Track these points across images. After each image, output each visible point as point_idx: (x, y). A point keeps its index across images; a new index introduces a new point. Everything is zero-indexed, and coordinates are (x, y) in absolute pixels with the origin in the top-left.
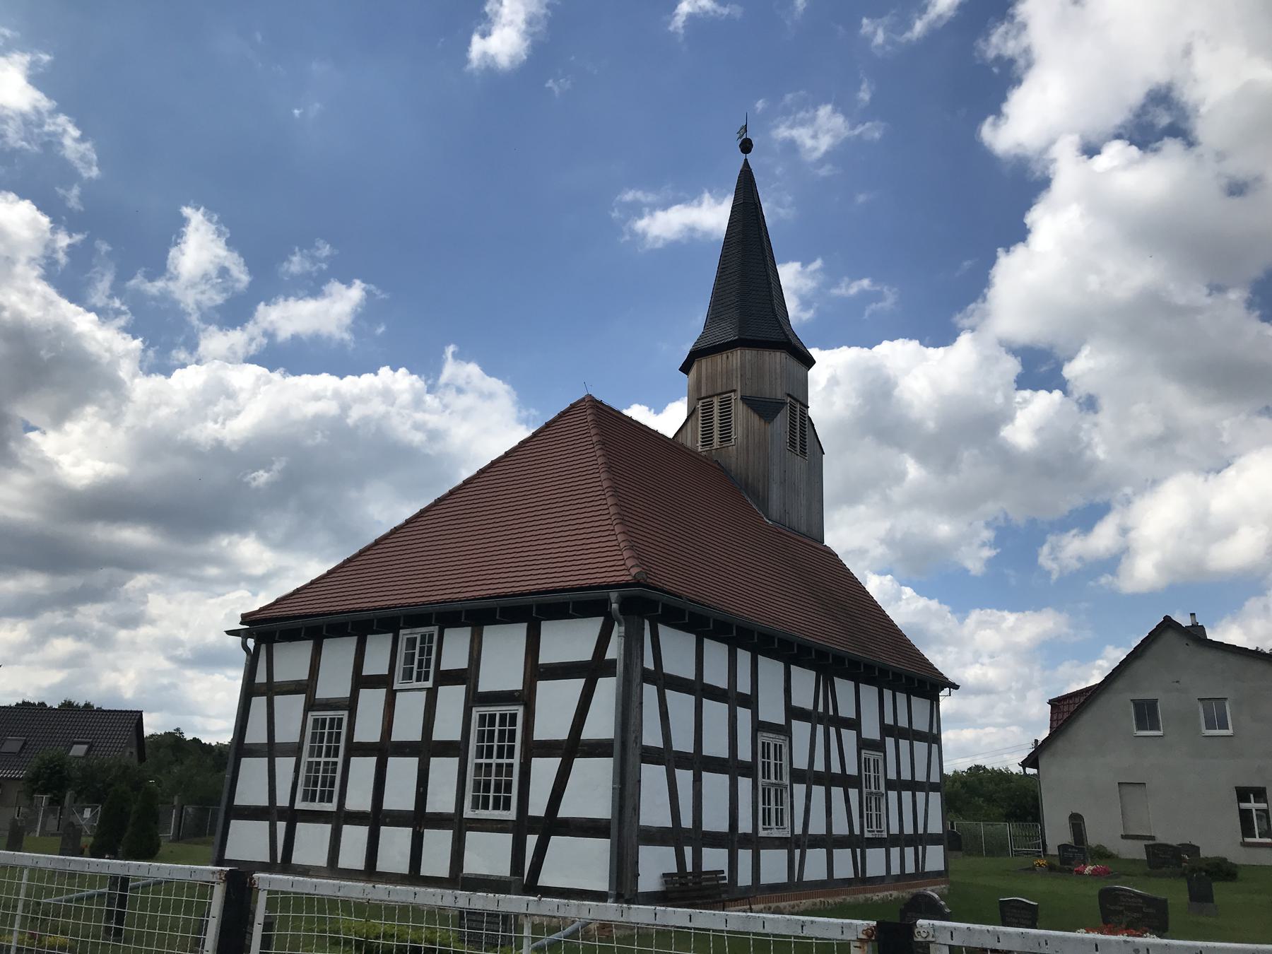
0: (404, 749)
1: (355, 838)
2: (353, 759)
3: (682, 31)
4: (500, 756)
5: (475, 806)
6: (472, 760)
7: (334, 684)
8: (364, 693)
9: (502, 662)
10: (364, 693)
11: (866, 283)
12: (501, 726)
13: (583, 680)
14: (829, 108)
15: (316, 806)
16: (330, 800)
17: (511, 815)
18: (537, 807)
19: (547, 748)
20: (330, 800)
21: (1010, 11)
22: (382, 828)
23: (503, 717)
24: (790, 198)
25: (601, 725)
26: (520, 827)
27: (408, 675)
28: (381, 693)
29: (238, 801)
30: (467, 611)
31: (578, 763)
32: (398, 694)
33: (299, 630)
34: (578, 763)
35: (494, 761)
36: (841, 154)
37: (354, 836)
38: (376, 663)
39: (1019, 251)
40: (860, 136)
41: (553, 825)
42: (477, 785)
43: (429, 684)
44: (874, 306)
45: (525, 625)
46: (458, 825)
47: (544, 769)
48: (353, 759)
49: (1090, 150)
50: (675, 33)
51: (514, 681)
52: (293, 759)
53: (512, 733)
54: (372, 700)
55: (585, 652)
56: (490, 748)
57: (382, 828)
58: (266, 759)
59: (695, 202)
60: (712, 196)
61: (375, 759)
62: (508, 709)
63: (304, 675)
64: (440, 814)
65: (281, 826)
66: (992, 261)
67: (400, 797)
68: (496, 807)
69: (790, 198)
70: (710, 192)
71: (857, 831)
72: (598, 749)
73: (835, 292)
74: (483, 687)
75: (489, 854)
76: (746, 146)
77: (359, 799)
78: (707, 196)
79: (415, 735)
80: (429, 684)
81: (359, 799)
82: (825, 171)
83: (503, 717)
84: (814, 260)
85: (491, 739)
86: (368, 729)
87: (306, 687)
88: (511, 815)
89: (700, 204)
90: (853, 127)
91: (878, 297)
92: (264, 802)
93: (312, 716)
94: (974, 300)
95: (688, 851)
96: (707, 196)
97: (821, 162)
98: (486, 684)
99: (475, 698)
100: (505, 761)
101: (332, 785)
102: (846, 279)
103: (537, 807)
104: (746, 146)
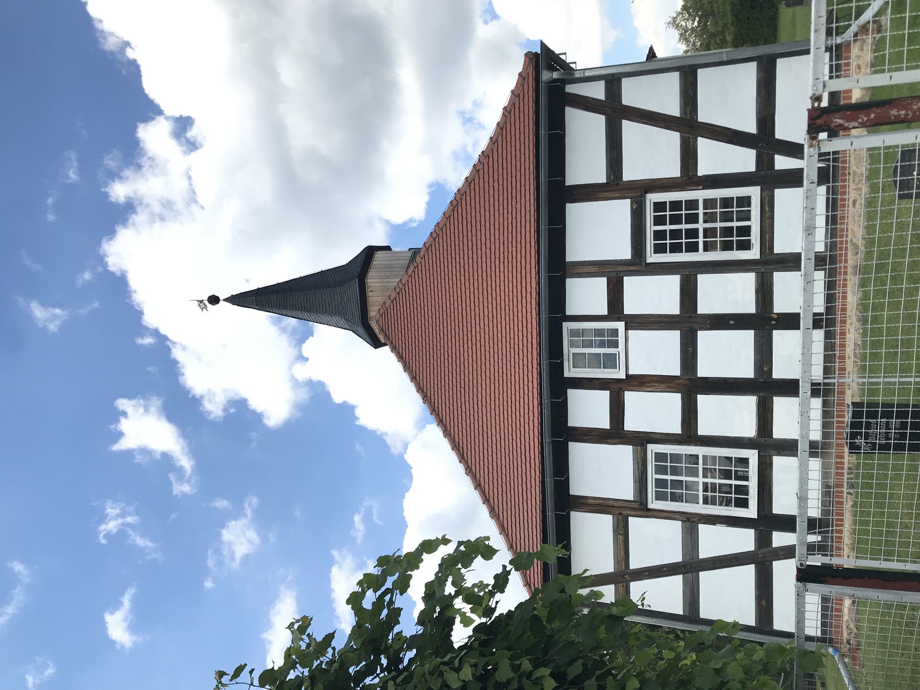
2: (701, 432)
3: (134, 638)
5: (744, 504)
6: (701, 256)
8: (631, 424)
10: (631, 424)
11: (357, 518)
14: (224, 532)
17: (752, 455)
18: (743, 160)
20: (744, 462)
21: (198, 396)
22: (776, 375)
24: (282, 571)
26: (769, 179)
27: (610, 361)
28: (631, 398)
29: (751, 621)
30: (556, 510)
31: (704, 116)
32: (631, 372)
34: (704, 116)
36: (262, 522)
39: (358, 412)
40: (253, 511)
41: (764, 140)
43: (620, 326)
44: (375, 517)
45: (569, 390)
48: (701, 432)
49: (302, 358)
50: (135, 644)
51: (621, 209)
52: (702, 527)
55: (596, 123)
57: (776, 375)
58: (703, 575)
59: (267, 646)
60: (267, 631)
61: (700, 174)
66: (363, 429)
69: (282, 571)
70: (263, 632)
72: (689, 156)
73: (359, 539)
74: (625, 253)
75: (796, 219)
76: (214, 300)
78: (265, 636)
80: (620, 326)
82: (272, 538)
84: (333, 556)
87: (620, 513)
88: (752, 455)
89: (270, 642)
90: (246, 515)
91: (369, 511)
92: (748, 572)
93: (654, 504)
94: (384, 441)
96: (265, 636)
97: (264, 539)
98: (626, 491)
99: (638, 265)
102: (352, 532)
103: (743, 160)
104: (214, 300)
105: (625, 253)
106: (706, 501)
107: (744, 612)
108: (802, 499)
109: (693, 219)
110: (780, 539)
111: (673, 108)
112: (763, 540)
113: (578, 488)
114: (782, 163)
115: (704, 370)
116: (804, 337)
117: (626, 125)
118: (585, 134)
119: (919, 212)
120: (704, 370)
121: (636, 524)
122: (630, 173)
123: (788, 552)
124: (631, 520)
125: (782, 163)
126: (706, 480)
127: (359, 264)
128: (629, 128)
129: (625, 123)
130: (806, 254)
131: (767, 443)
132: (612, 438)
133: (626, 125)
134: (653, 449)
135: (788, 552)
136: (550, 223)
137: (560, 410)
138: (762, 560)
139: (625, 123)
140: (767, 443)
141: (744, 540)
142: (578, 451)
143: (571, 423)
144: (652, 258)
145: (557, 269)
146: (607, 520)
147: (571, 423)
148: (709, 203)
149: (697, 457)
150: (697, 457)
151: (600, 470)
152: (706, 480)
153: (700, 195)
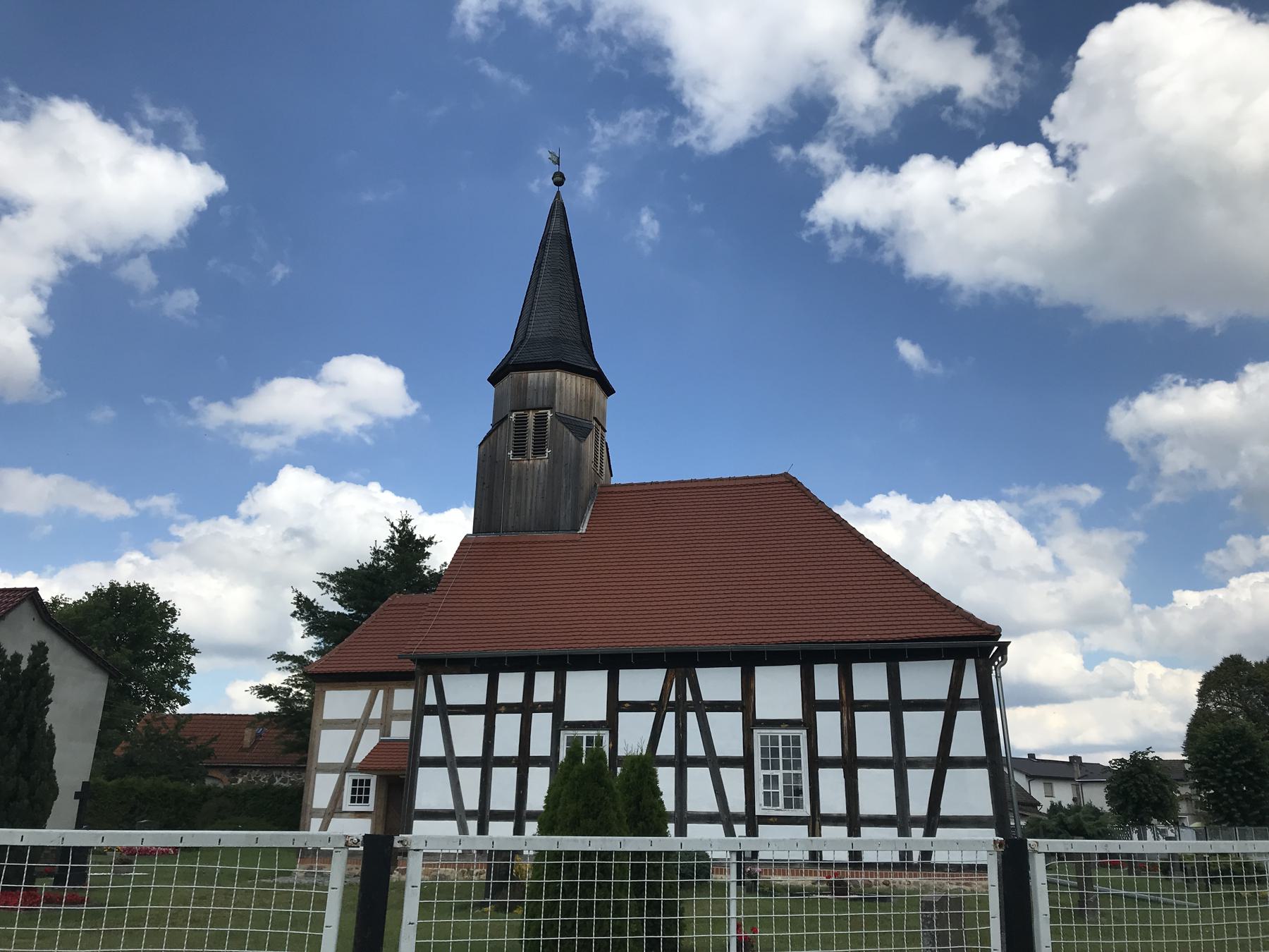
6: (759, 774)
10: (820, 716)
17: (806, 811)
20: (799, 805)
31: (951, 774)
34: (951, 774)
45: (739, 669)
54: (828, 724)
74: (569, 716)
76: (559, 180)
87: (745, 705)
104: (559, 180)
107: (423, 800)
110: (472, 825)
112: (471, 815)
113: (763, 675)
117: (651, 716)
118: (926, 680)
119: (496, 950)
121: (737, 717)
122: (798, 715)
124: (325, 717)
126: (775, 772)
128: (939, 716)
131: (816, 821)
134: (803, 734)
136: (873, 651)
137: (586, 662)
139: (942, 714)
141: (737, 804)
142: (602, 677)
143: (816, 667)
144: (758, 734)
145: (747, 661)
146: (737, 697)
147: (816, 667)
148: (798, 777)
151: (778, 691)
152: (775, 772)
153: (804, 771)
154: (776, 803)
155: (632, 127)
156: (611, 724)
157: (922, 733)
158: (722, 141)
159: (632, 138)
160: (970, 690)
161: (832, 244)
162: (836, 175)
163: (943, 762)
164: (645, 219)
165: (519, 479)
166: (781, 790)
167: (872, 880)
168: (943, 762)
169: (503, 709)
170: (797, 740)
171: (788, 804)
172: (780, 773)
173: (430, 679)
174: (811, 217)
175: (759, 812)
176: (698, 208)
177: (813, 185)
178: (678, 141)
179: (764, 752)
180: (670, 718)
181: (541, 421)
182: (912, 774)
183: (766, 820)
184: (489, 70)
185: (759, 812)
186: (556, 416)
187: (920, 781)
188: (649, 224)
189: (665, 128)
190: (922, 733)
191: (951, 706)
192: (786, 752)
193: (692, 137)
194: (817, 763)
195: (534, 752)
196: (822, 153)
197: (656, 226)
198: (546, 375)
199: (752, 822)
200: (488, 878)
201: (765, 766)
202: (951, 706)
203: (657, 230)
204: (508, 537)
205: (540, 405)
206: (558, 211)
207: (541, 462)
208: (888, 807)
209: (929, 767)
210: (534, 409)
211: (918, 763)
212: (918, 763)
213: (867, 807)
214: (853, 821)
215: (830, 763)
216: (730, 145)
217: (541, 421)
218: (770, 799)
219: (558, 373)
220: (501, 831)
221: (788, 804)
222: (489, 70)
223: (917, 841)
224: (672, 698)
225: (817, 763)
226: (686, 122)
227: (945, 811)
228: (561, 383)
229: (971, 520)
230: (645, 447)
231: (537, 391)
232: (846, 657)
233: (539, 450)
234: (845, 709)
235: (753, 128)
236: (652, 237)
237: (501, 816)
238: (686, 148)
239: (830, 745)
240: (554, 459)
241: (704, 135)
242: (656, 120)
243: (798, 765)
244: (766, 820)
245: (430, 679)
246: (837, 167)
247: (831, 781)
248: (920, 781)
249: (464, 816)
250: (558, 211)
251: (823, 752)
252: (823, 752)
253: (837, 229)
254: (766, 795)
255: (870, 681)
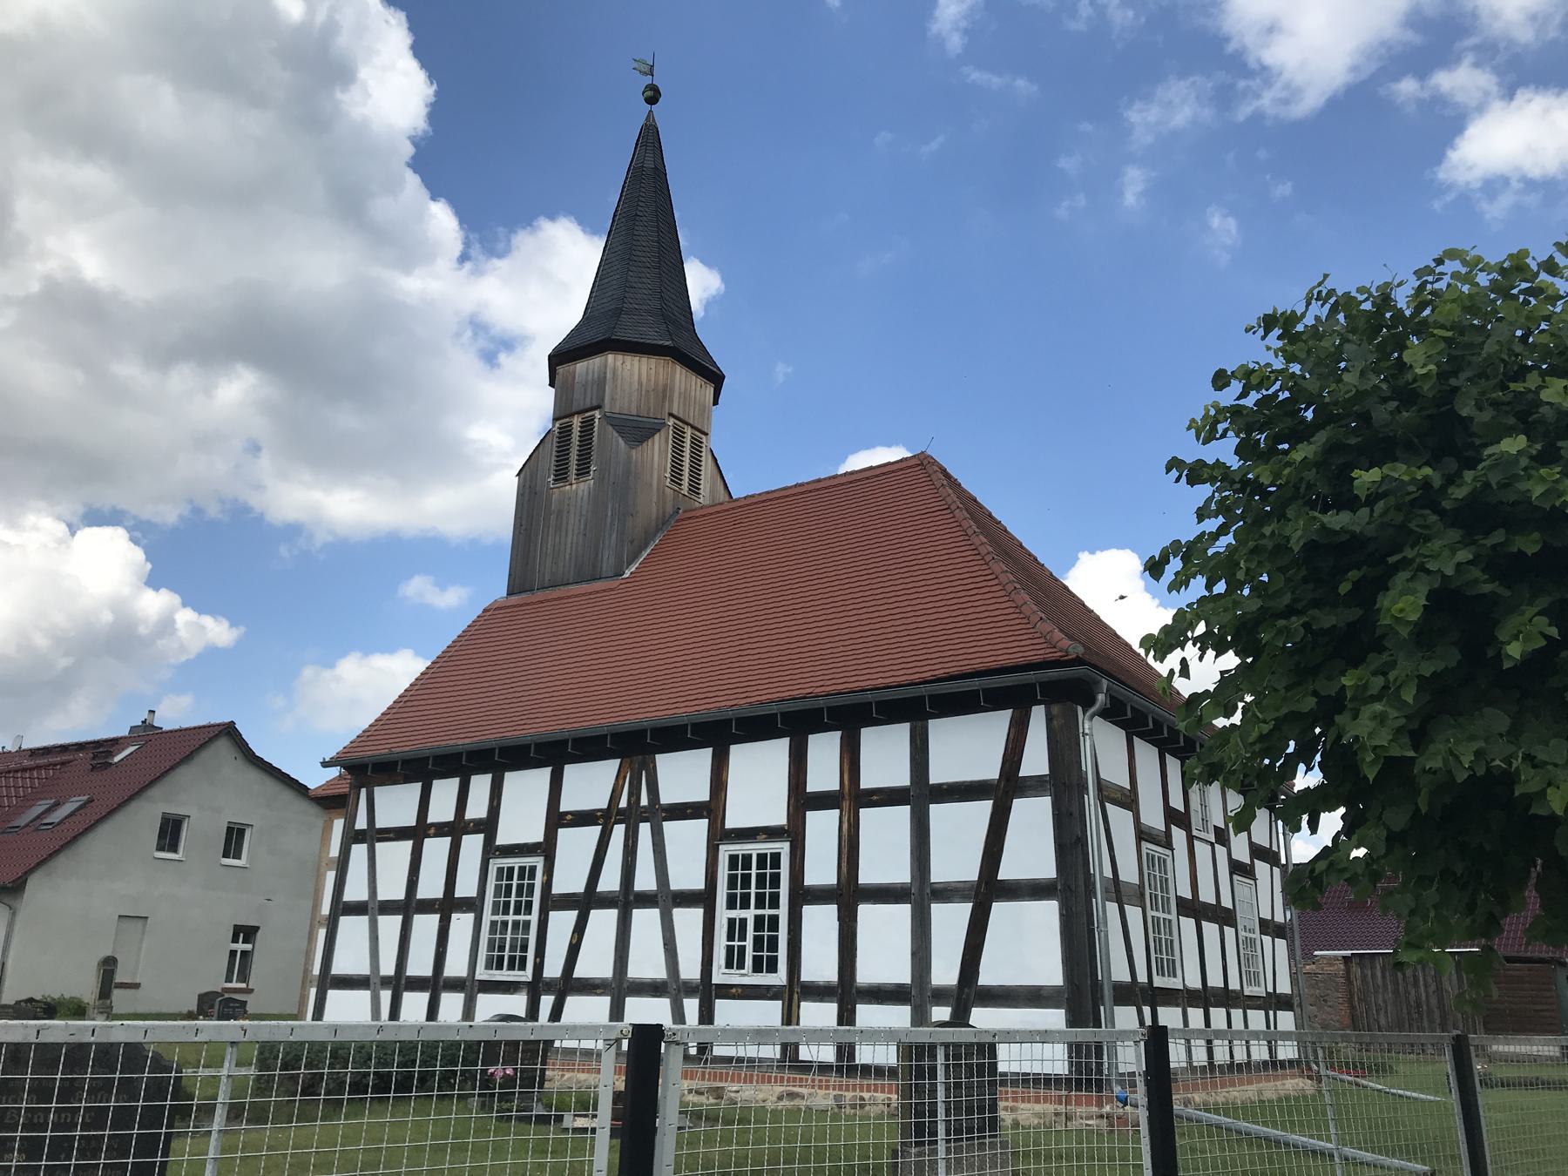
0: (427, 906)
1: (819, 1015)
2: (806, 909)
4: (517, 912)
6: (723, 915)
7: (522, 819)
9: (523, 803)
12: (521, 880)
13: (990, 803)
15: (504, 975)
16: (523, 967)
17: (780, 978)
18: (553, 969)
19: (566, 902)
20: (773, 968)
23: (522, 869)
25: (1031, 848)
26: (536, 988)
31: (999, 909)
33: (974, 694)
34: (999, 909)
35: (511, 918)
37: (819, 1015)
38: (824, 773)
42: (491, 943)
45: (839, 733)
46: (470, 987)
47: (562, 923)
48: (806, 909)
53: (531, 887)
54: (822, 827)
56: (507, 904)
62: (527, 861)
63: (703, 795)
64: (587, 979)
65: (386, 996)
67: (596, 962)
68: (511, 967)
71: (1142, 977)
74: (731, 822)
76: (653, 96)
77: (820, 964)
79: (399, 894)
81: (820, 964)
83: (522, 869)
85: (508, 894)
86: (570, 877)
87: (711, 809)
93: (725, 851)
95: (1147, 1010)
98: (735, 818)
100: (522, 918)
101: (525, 948)
103: (553, 969)
104: (653, 96)
105: (731, 822)
106: (493, 923)
108: (1044, 1037)
109: (760, 904)
110: (691, 1006)
111: (1008, 871)
112: (689, 989)
113: (740, 755)
114: (547, 1002)
115: (865, 912)
116: (1059, 1032)
117: (408, 844)
120: (865, 912)
123: (679, 1016)
125: (547, 1002)
127: (552, 446)
129: (410, 843)
130: (301, 1027)
131: (796, 992)
132: (797, 800)
133: (408, 844)
134: (784, 848)
135: (679, 1016)
138: (669, 988)
140: (796, 992)
142: (777, 751)
145: (718, 735)
146: (703, 795)
147: (733, 748)
148: (774, 921)
149: (777, 907)
150: (777, 907)
151: (758, 782)
153: (783, 912)
154: (741, 966)
155: (1176, 107)
156: (794, 833)
157: (958, 838)
158: (1311, 101)
159: (1182, 116)
160: (1035, 762)
161: (1485, 206)
162: (1481, 109)
163: (988, 890)
164: (1216, 222)
165: (560, 513)
166: (749, 944)
167: (866, 1095)
168: (988, 890)
169: (432, 831)
170: (776, 858)
171: (757, 968)
172: (750, 914)
173: (363, 791)
174: (1442, 175)
175: (717, 979)
176: (1284, 190)
177: (1449, 122)
178: (1243, 112)
179: (732, 882)
180: (619, 831)
181: (587, 426)
182: (938, 911)
183: (727, 991)
184: (976, 76)
185: (717, 979)
186: (605, 416)
187: (950, 921)
188: (1222, 226)
189: (1224, 98)
190: (958, 838)
191: (1004, 790)
192: (746, 880)
193: (1266, 101)
194: (803, 895)
195: (831, 911)
196: (1461, 80)
197: (1232, 223)
198: (595, 363)
199: (708, 992)
200: (543, 1071)
201: (731, 904)
202: (1004, 790)
203: (1234, 230)
204: (540, 595)
205: (588, 405)
206: (649, 139)
207: (580, 489)
208: (899, 972)
209: (964, 899)
210: (578, 413)
211: (947, 893)
212: (947, 893)
213: (868, 972)
214: (847, 993)
215: (820, 896)
216: (1323, 100)
217: (587, 426)
218: (734, 959)
219: (610, 357)
220: (415, 1005)
221: (757, 968)
222: (976, 76)
223: (695, 1031)
224: (623, 804)
225: (803, 895)
226: (1255, 83)
227: (986, 978)
228: (614, 371)
229: (1192, 481)
230: (758, 446)
231: (585, 386)
232: (850, 717)
233: (583, 471)
234: (846, 804)
235: (1354, 69)
236: (1229, 242)
237: (818, 992)
238: (1258, 117)
239: (821, 869)
240: (600, 481)
241: (1283, 95)
242: (1210, 85)
243: (775, 903)
244: (727, 991)
245: (363, 791)
246: (1487, 94)
247: (820, 922)
248: (950, 921)
249: (1296, 1001)
250: (649, 139)
251: (812, 878)
252: (812, 878)
253: (1494, 185)
254: (730, 950)
255: (885, 756)
